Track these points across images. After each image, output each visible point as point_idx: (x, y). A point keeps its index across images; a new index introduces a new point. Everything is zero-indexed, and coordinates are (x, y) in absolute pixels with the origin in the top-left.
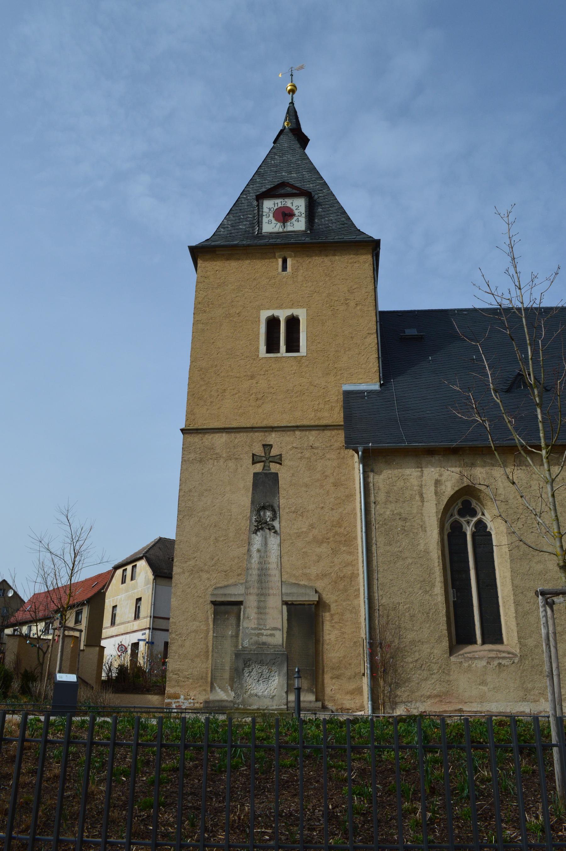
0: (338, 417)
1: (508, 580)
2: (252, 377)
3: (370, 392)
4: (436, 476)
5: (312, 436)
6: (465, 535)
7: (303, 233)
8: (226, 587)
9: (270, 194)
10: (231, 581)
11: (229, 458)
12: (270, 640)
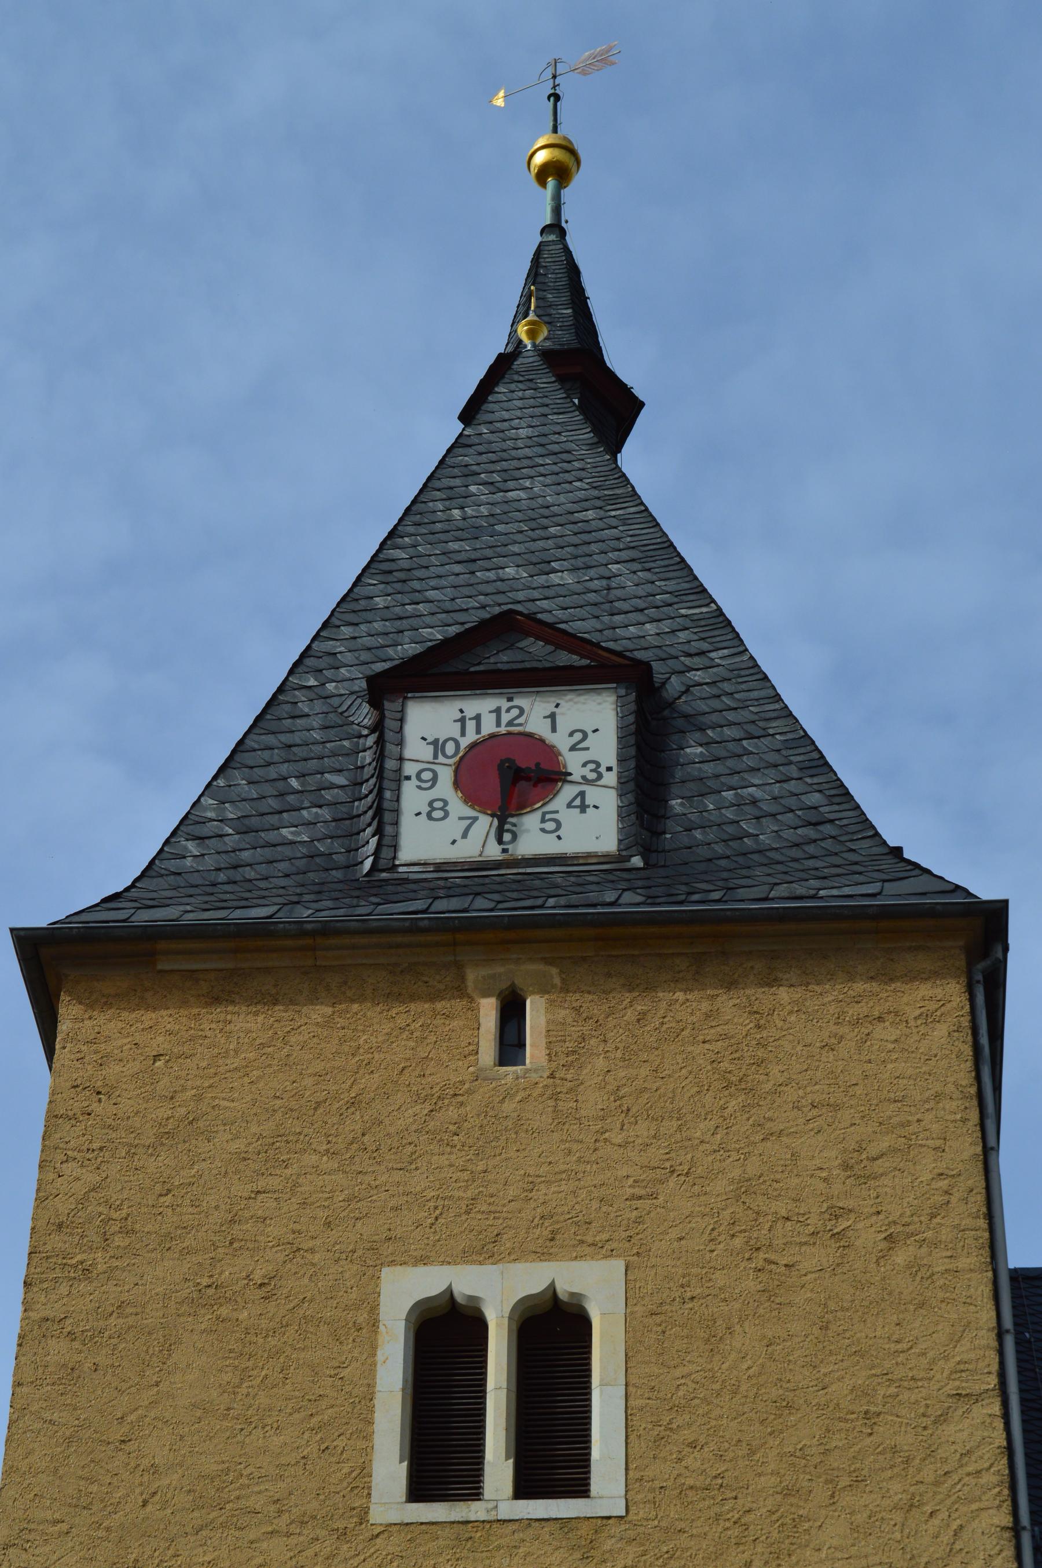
7: (609, 868)
9: (440, 670)
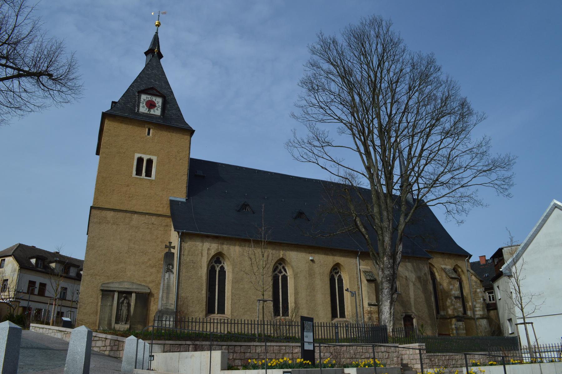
0: (167, 212)
1: (230, 290)
2: (128, 186)
3: (182, 202)
4: (208, 247)
5: (154, 219)
6: (216, 271)
8: (108, 283)
10: (111, 281)
11: (114, 224)
12: (170, 307)
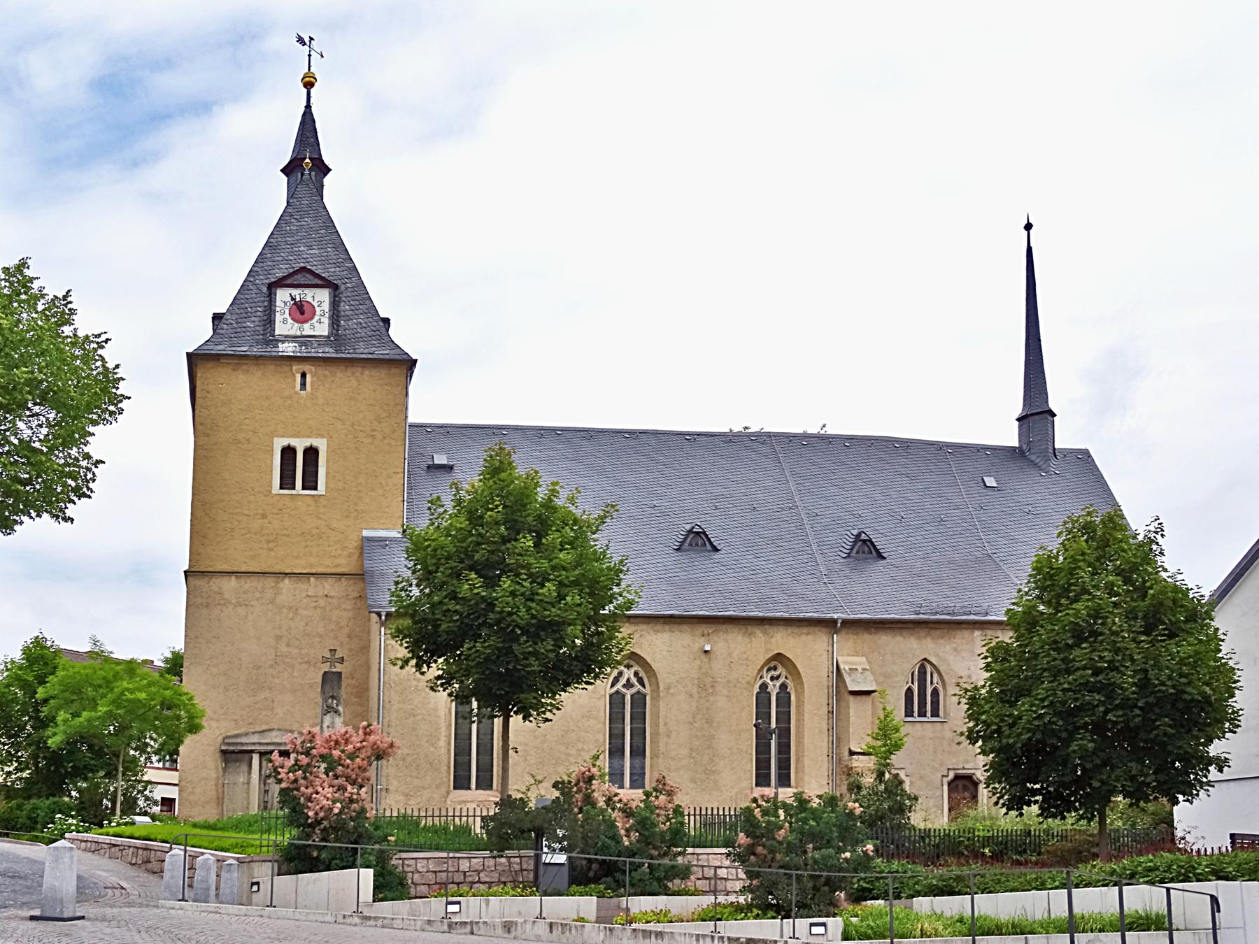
9: (281, 283)
